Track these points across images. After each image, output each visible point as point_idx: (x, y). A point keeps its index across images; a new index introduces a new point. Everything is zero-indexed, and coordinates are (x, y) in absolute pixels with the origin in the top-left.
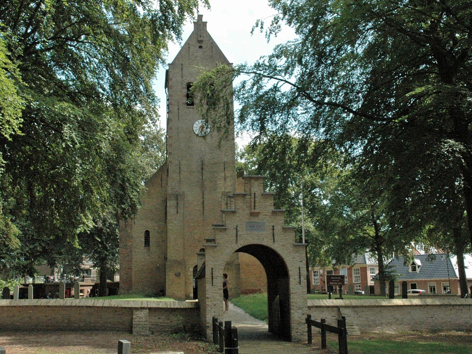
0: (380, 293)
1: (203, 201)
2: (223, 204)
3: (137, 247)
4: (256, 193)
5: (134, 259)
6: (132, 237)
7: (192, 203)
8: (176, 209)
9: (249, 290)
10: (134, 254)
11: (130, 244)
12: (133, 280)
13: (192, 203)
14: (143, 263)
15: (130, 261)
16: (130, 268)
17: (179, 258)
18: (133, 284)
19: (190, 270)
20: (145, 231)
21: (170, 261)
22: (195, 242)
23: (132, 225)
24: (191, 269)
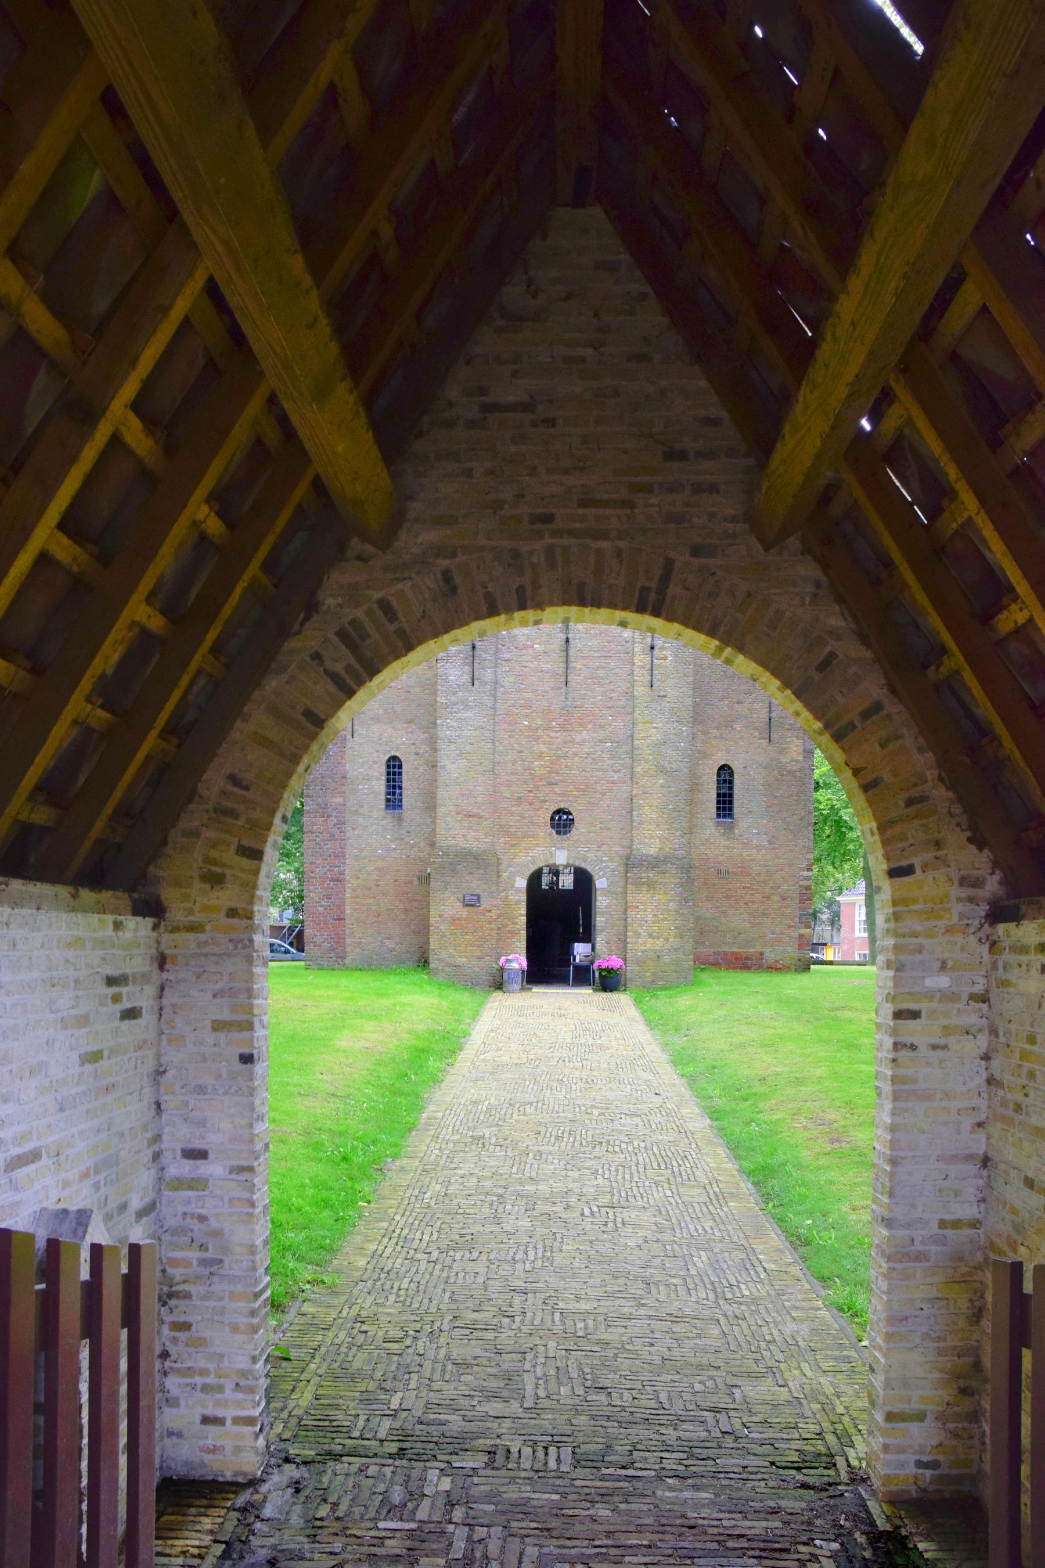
0: (442, 843)
1: (567, 641)
2: (638, 648)
3: (361, 811)
4: (765, 742)
5: (351, 851)
6: (344, 777)
7: (526, 647)
8: (467, 669)
9: (725, 954)
10: (350, 833)
11: (338, 800)
12: (347, 917)
13: (526, 647)
14: (380, 864)
15: (341, 855)
16: (339, 880)
17: (478, 840)
18: (348, 932)
19: (517, 885)
20: (387, 758)
21: (445, 854)
22: (537, 787)
23: (344, 739)
24: (522, 883)
